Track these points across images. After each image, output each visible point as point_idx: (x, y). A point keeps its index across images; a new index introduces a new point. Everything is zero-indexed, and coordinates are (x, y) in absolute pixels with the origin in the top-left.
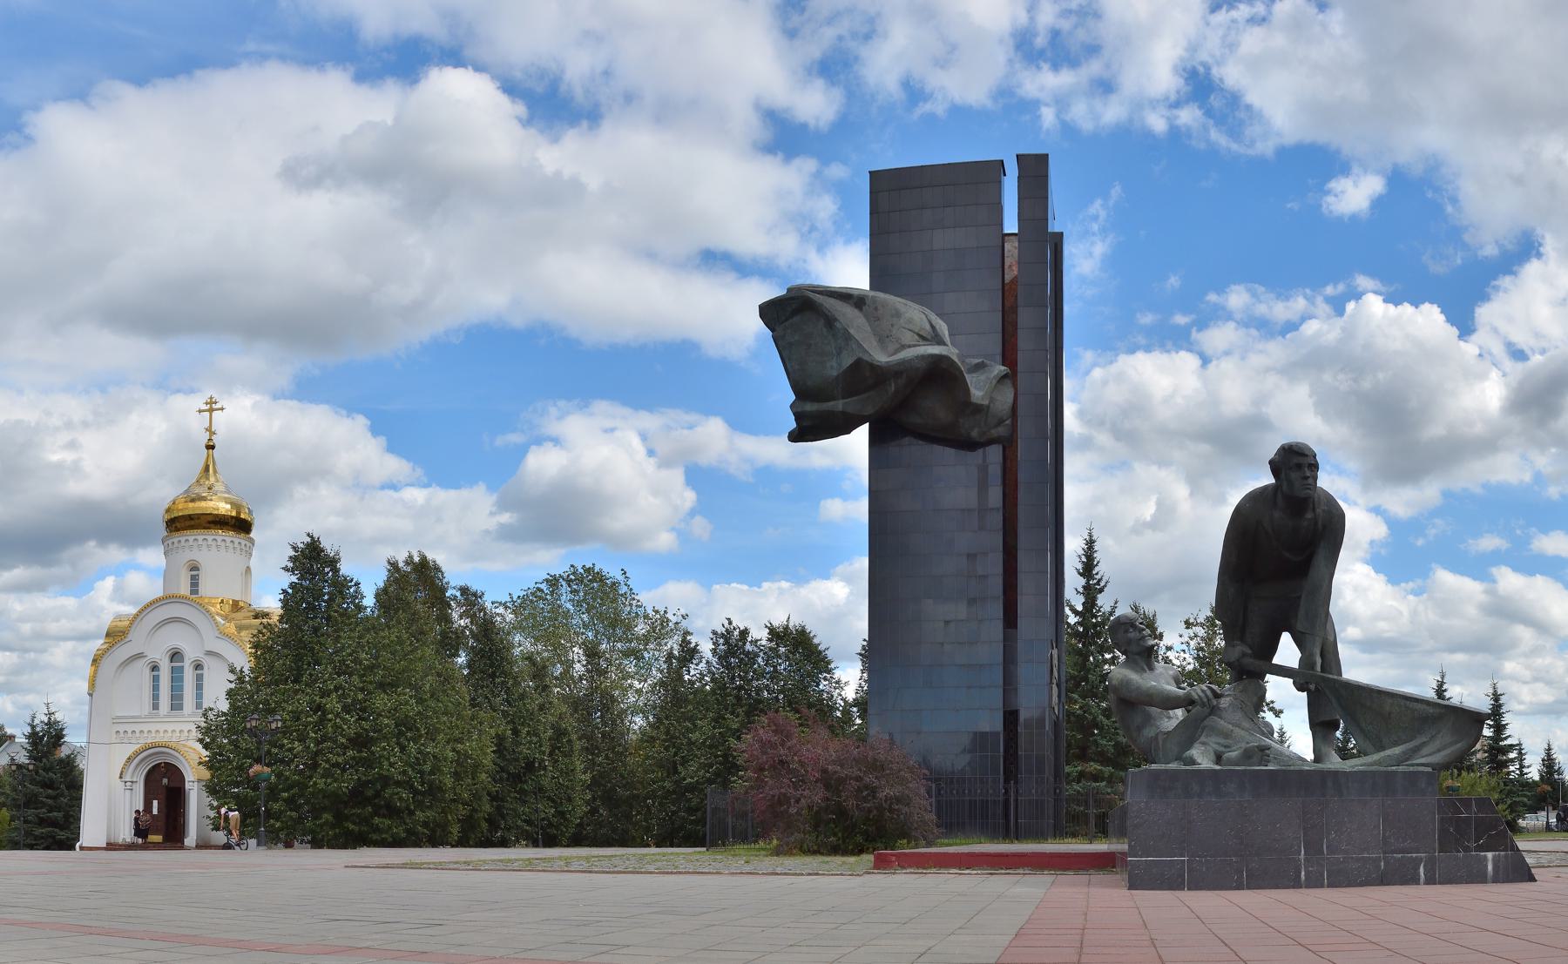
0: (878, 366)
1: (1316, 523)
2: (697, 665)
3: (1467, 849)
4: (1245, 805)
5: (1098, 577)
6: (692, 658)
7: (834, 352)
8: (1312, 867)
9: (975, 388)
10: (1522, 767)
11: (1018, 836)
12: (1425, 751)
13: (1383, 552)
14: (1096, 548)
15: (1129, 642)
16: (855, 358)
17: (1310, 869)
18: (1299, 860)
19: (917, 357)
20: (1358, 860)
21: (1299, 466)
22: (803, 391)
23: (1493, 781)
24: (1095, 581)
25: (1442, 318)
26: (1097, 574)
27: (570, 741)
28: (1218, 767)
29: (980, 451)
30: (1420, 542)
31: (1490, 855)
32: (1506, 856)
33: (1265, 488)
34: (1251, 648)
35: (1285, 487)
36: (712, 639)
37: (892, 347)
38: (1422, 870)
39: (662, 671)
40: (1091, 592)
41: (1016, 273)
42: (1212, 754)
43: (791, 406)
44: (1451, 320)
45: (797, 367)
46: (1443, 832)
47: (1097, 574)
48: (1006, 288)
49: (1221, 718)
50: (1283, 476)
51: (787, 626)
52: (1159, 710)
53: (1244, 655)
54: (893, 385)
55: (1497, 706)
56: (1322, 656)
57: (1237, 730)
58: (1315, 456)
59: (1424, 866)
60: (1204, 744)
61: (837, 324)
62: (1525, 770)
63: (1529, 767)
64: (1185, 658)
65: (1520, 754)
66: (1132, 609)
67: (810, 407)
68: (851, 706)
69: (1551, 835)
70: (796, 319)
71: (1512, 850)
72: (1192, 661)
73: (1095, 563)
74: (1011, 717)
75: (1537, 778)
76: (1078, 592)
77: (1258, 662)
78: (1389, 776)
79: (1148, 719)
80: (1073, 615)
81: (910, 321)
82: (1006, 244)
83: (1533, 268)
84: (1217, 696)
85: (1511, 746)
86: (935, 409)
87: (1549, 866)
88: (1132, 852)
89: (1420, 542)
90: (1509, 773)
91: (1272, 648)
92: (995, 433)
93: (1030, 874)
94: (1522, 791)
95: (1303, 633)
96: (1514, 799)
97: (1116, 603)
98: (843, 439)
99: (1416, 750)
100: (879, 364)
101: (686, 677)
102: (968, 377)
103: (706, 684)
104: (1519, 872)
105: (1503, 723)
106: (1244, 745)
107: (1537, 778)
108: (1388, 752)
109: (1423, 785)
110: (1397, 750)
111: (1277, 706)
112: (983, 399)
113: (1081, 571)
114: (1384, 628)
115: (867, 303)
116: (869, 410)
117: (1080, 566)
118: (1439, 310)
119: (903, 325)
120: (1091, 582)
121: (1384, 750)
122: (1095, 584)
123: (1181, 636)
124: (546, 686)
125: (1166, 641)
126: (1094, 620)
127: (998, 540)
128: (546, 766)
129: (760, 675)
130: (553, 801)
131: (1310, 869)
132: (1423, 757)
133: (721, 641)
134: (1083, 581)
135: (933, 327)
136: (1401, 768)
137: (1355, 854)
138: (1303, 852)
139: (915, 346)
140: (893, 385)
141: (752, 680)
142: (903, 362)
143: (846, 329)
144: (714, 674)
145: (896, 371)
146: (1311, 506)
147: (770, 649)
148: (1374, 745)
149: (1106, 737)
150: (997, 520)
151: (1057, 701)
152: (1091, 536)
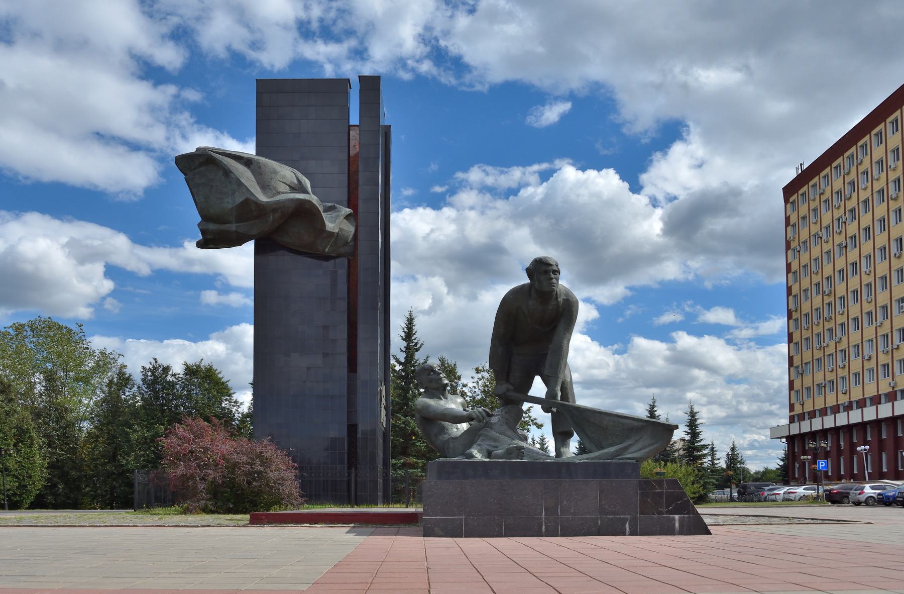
0: (261, 204)
2: (131, 389)
3: (660, 513)
4: (505, 484)
5: (415, 341)
6: (128, 383)
7: (230, 193)
8: (550, 523)
9: (329, 221)
10: (713, 459)
11: (357, 503)
12: (632, 449)
13: (595, 327)
14: (414, 323)
15: (431, 381)
16: (244, 198)
17: (549, 524)
18: (541, 519)
22: (206, 217)
23: (690, 469)
24: (414, 344)
25: (617, 177)
26: (415, 339)
27: (30, 437)
28: (487, 460)
29: (332, 261)
30: (620, 320)
31: (677, 517)
32: (689, 518)
33: (523, 286)
35: (537, 285)
38: (627, 526)
39: (104, 393)
40: (411, 349)
41: (358, 150)
42: (485, 451)
43: (198, 225)
44: (623, 178)
47: (415, 339)
48: (351, 159)
49: (492, 429)
50: (535, 278)
51: (199, 365)
52: (450, 424)
53: (508, 390)
54: (271, 217)
57: (502, 437)
60: (479, 445)
61: (233, 176)
62: (716, 462)
63: (718, 459)
64: (475, 392)
66: (440, 360)
67: (212, 227)
68: (246, 418)
69: (732, 504)
70: (202, 169)
72: (480, 393)
73: (414, 333)
74: (352, 429)
75: (724, 466)
77: (517, 395)
78: (604, 466)
79: (443, 430)
80: (398, 365)
81: (284, 177)
82: (351, 132)
83: (678, 149)
84: (489, 415)
86: (299, 234)
87: (723, 525)
88: (426, 512)
89: (620, 320)
90: (701, 464)
91: (529, 386)
92: (342, 250)
93: (358, 527)
94: (711, 475)
95: (548, 376)
96: (706, 480)
97: (427, 358)
99: (625, 449)
102: (324, 215)
103: (138, 402)
104: (702, 529)
105: (698, 431)
106: (507, 447)
107: (724, 466)
108: (605, 451)
110: (612, 449)
111: (539, 422)
112: (333, 229)
113: (404, 337)
114: (600, 374)
116: (255, 231)
117: (403, 334)
118: (614, 172)
120: (411, 344)
121: (603, 449)
122: (413, 346)
123: (473, 378)
124: (12, 399)
125: (463, 381)
126: (413, 368)
128: (11, 454)
130: (17, 478)
131: (549, 524)
133: (149, 374)
134: (405, 344)
136: (614, 461)
138: (544, 514)
140: (271, 217)
141: (172, 400)
142: (278, 202)
144: (143, 395)
145: (276, 208)
148: (596, 446)
149: (420, 441)
150: (343, 305)
151: (385, 419)
152: (411, 315)
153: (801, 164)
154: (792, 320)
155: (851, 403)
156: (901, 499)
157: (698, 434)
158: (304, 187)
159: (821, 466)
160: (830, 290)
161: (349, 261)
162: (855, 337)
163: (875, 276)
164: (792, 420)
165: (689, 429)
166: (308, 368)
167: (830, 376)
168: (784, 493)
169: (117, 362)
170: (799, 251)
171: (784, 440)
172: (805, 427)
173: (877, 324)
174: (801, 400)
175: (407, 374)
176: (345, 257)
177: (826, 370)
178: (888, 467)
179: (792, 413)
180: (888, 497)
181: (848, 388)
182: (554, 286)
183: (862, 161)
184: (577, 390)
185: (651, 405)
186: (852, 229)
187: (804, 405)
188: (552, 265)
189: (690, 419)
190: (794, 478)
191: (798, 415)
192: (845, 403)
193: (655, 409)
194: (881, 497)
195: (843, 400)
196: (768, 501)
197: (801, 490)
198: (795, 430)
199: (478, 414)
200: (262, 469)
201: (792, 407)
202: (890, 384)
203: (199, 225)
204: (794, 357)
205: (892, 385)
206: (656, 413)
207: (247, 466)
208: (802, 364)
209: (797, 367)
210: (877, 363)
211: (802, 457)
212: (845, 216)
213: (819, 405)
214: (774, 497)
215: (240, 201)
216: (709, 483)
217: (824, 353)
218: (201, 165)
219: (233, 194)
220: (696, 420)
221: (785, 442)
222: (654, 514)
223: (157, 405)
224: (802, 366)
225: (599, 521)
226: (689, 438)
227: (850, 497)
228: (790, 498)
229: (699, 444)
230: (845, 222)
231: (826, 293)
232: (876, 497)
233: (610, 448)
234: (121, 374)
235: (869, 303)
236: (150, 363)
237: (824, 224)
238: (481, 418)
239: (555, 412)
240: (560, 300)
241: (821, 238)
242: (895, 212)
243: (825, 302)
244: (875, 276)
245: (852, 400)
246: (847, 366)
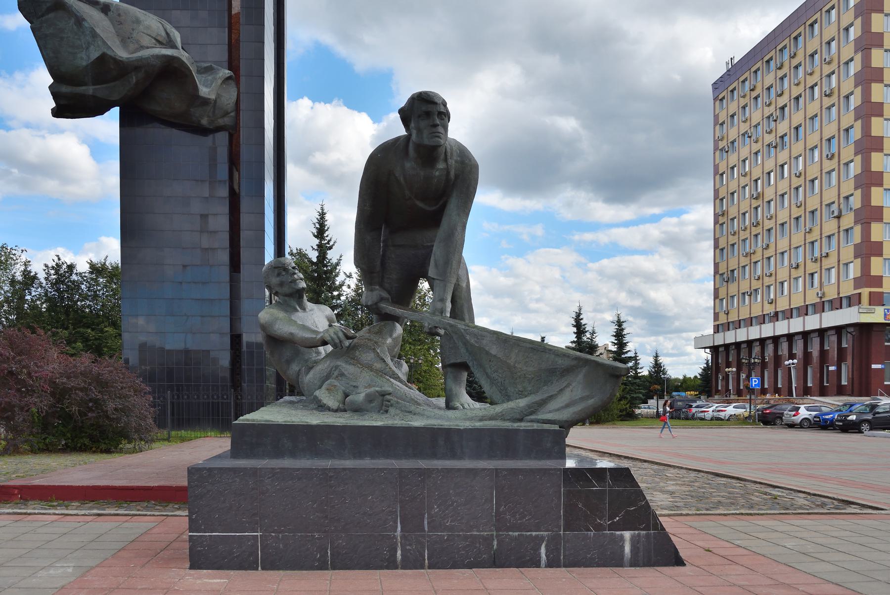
1: (448, 173)
3: (599, 528)
5: (328, 239)
7: (84, 46)
8: (410, 545)
12: (553, 405)
14: (326, 218)
17: (408, 547)
18: (395, 537)
20: (466, 538)
21: (428, 114)
24: (326, 242)
26: (327, 236)
29: (211, 137)
31: (627, 535)
32: (647, 536)
33: (397, 139)
34: (389, 293)
36: (45, 270)
38: (543, 550)
46: (570, 508)
47: (327, 236)
53: (382, 299)
54: (134, 77)
55: (620, 330)
56: (453, 301)
58: (445, 104)
59: (546, 546)
61: (86, 25)
63: (641, 368)
65: (637, 364)
67: (65, 89)
71: (655, 528)
73: (326, 229)
74: (236, 339)
76: (314, 249)
81: (148, 27)
85: (630, 358)
92: (221, 122)
94: (638, 389)
95: (434, 279)
96: (632, 395)
97: (341, 257)
98: (98, 119)
99: (542, 403)
100: (121, 59)
101: (28, 297)
105: (625, 341)
109: (549, 445)
110: (522, 403)
113: (316, 234)
115: (112, 9)
117: (315, 231)
119: (143, 31)
120: (323, 242)
122: (326, 244)
129: (85, 297)
131: (408, 547)
132: (550, 412)
133: (53, 272)
134: (317, 241)
135: (167, 34)
137: (462, 530)
139: (153, 47)
140: (134, 77)
142: (141, 59)
143: (92, 28)
146: (442, 156)
147: (92, 279)
152: (322, 210)
153: (731, 59)
154: (718, 225)
155: (776, 314)
156: (841, 424)
157: (625, 344)
158: (172, 41)
159: (754, 383)
161: (231, 136)
163: (805, 178)
164: (717, 329)
165: (616, 340)
166: (185, 266)
168: (713, 411)
169: (21, 258)
171: (708, 350)
172: (730, 337)
173: (806, 229)
175: (319, 276)
176: (226, 130)
177: (752, 278)
178: (813, 382)
179: (717, 323)
180: (826, 420)
182: (439, 137)
183: (795, 54)
184: (477, 300)
185: (576, 313)
187: (729, 315)
188: (435, 103)
189: (617, 329)
190: (717, 391)
192: (771, 313)
193: (581, 317)
194: (818, 420)
195: (769, 309)
196: (696, 419)
197: (731, 410)
198: (719, 340)
199: (335, 337)
200: (100, 396)
201: (716, 316)
203: (50, 87)
205: (820, 295)
206: (582, 321)
207: (81, 394)
208: (727, 271)
209: (722, 274)
210: (805, 271)
211: (727, 370)
212: (776, 113)
214: (703, 414)
216: (636, 398)
219: (87, 48)
220: (623, 330)
221: (709, 352)
222: (591, 531)
223: (63, 306)
224: (728, 273)
225: (495, 543)
226: (615, 349)
227: (784, 418)
228: (719, 416)
229: (626, 355)
231: (755, 197)
232: (812, 420)
233: (519, 400)
234: (26, 273)
235: (798, 207)
236: (53, 260)
238: (337, 341)
239: (443, 334)
240: (452, 162)
242: (798, 249)
244: (805, 178)
246: (774, 274)
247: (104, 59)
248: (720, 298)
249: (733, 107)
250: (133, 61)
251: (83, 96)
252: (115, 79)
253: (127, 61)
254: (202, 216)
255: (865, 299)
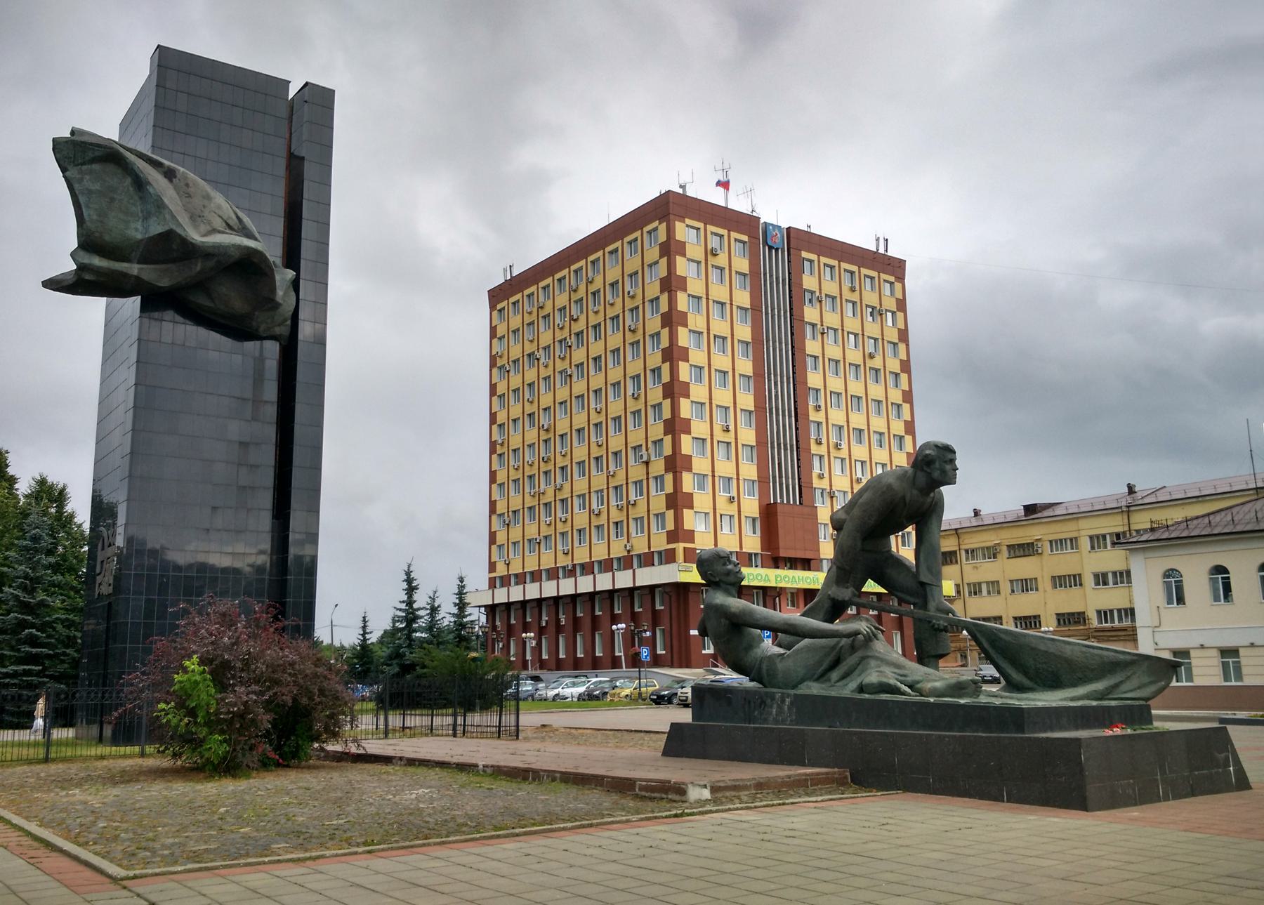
0: (191, 243)
12: (1124, 687)
16: (166, 228)
19: (233, 245)
22: (88, 243)
37: (203, 228)
45: (95, 217)
61: (151, 190)
70: (96, 167)
81: (219, 207)
92: (277, 330)
100: (194, 241)
115: (178, 176)
127: (271, 432)
135: (238, 217)
142: (218, 247)
150: (271, 412)
160: (550, 425)
162: (581, 485)
164: (492, 584)
167: (545, 531)
170: (508, 371)
171: (482, 610)
174: (506, 558)
179: (493, 575)
181: (570, 547)
186: (579, 355)
191: (501, 578)
195: (563, 561)
201: (492, 567)
202: (626, 546)
203: (73, 255)
204: (498, 503)
211: (524, 635)
213: (531, 566)
215: (157, 233)
217: (539, 500)
218: (94, 160)
230: (570, 347)
237: (542, 344)
241: (538, 360)
243: (542, 438)
245: (575, 562)
247: (169, 237)
248: (498, 543)
249: (516, 322)
250: (208, 247)
251: (125, 275)
252: (174, 261)
253: (201, 245)
254: (241, 443)
255: (680, 555)
